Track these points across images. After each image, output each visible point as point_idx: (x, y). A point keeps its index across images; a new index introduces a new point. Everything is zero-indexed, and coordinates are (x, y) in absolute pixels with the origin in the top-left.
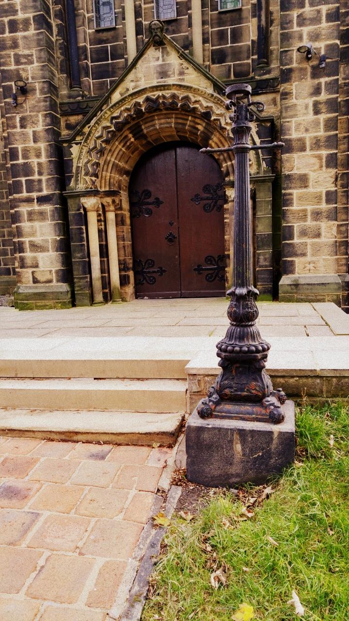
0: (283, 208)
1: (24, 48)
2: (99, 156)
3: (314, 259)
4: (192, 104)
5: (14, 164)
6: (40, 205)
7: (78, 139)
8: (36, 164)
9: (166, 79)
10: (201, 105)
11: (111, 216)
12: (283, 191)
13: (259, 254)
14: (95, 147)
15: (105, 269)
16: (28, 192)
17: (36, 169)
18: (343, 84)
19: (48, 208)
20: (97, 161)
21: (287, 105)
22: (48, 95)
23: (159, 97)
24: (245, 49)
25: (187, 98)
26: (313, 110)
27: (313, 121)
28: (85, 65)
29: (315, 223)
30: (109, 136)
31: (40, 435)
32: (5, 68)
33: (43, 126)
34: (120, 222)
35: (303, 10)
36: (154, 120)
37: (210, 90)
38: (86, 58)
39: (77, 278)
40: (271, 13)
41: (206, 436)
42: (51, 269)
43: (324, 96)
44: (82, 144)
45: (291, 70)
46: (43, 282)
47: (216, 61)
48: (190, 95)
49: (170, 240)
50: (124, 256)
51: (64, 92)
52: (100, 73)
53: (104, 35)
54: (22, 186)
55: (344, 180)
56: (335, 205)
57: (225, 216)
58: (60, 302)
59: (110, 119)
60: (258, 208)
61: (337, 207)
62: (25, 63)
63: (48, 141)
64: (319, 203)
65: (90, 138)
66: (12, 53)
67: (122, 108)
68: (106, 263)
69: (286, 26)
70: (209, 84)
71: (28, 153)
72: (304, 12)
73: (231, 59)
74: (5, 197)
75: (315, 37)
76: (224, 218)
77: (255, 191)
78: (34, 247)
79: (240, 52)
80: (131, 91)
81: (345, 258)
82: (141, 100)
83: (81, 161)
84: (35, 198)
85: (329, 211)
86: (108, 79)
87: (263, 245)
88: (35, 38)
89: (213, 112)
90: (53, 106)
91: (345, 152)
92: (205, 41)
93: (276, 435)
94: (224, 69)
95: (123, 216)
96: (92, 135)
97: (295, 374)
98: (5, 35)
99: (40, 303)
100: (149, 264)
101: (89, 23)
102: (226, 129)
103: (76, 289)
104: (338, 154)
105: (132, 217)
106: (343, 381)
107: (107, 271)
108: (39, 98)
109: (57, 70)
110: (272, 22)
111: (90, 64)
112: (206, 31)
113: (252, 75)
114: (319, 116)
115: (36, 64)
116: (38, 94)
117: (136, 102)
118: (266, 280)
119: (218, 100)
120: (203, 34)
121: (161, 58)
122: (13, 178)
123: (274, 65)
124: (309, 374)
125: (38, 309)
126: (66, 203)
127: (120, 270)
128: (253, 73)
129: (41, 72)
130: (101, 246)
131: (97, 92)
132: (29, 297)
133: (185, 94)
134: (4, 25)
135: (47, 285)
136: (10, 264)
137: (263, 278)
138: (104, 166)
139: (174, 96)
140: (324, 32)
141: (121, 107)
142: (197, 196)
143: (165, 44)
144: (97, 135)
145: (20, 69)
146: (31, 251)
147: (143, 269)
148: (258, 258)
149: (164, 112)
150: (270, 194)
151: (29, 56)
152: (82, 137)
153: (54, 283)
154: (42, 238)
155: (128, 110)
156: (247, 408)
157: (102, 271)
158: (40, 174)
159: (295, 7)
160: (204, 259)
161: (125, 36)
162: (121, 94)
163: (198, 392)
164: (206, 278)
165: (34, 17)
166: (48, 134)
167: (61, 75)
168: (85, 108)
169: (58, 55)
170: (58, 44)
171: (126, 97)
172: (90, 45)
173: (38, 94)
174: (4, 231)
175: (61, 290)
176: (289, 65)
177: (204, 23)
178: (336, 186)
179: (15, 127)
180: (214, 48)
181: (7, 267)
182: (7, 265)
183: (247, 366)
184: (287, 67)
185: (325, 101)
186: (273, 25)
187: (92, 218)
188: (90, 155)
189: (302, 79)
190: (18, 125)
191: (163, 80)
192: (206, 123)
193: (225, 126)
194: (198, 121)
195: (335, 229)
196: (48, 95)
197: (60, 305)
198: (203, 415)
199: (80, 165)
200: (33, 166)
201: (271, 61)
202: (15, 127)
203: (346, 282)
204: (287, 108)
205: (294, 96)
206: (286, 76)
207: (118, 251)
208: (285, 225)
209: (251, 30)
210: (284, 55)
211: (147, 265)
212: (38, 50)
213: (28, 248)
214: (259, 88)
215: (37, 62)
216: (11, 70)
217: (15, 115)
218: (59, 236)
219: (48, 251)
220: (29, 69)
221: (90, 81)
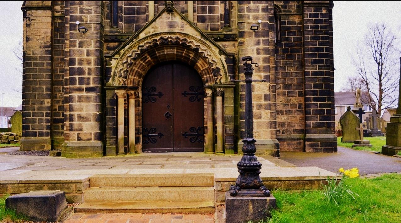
0: (240, 102)
2: (129, 67)
4: (188, 43)
5: (72, 68)
7: (116, 56)
8: (87, 68)
9: (173, 29)
10: (193, 44)
11: (132, 101)
12: (240, 93)
13: (226, 127)
14: (127, 62)
16: (79, 84)
18: (271, 41)
19: (93, 95)
20: (128, 69)
21: (242, 49)
22: (99, 31)
23: (168, 38)
24: (217, 17)
26: (257, 52)
27: (256, 58)
28: (121, 16)
29: (258, 111)
30: (136, 56)
31: (141, 211)
32: (73, 15)
34: (137, 104)
35: (249, 5)
36: (164, 49)
37: (199, 37)
38: (122, 13)
41: (236, 203)
42: (91, 132)
43: (261, 46)
44: (119, 59)
45: (244, 32)
46: (85, 140)
47: (200, 21)
48: (187, 39)
50: (138, 125)
55: (273, 89)
56: (269, 102)
57: (204, 104)
58: (96, 153)
59: (137, 46)
60: (225, 101)
61: (270, 103)
63: (96, 56)
64: (260, 100)
65: (124, 56)
66: (79, 7)
69: (241, 11)
71: (82, 62)
72: (250, 6)
73: (209, 21)
75: (257, 18)
76: (203, 106)
77: (224, 92)
78: (81, 118)
79: (214, 19)
80: (151, 33)
83: (117, 69)
84: (85, 88)
85: (266, 105)
86: (134, 24)
87: (229, 122)
90: (101, 37)
92: (194, 11)
94: (204, 25)
95: (139, 101)
96: (125, 55)
99: (82, 153)
100: (153, 131)
103: (107, 145)
104: (270, 75)
106: (291, 182)
108: (93, 32)
109: (104, 17)
111: (123, 15)
112: (195, 6)
113: (220, 31)
114: (259, 56)
115: (93, 14)
116: (93, 30)
117: (155, 39)
118: (230, 142)
119: (203, 42)
120: (194, 8)
121: (170, 18)
122: (70, 75)
123: (234, 27)
125: (80, 157)
126: (105, 93)
127: (136, 134)
129: (96, 19)
130: (125, 119)
131: (126, 30)
133: (184, 38)
136: (37, 129)
137: (229, 141)
138: (130, 72)
139: (177, 38)
141: (144, 41)
143: (173, 12)
144: (129, 55)
146: (78, 120)
152: (119, 56)
154: (87, 113)
155: (150, 43)
156: (253, 192)
158: (89, 74)
160: (189, 128)
162: (146, 34)
163: (221, 190)
164: (190, 140)
166: (97, 52)
167: (107, 20)
170: (106, 4)
171: (148, 36)
172: (124, 6)
174: (35, 107)
175: (97, 145)
176: (243, 29)
178: (270, 91)
179: (75, 46)
180: (199, 15)
181: (35, 131)
182: (34, 130)
184: (242, 30)
185: (262, 48)
186: (233, 9)
187: (121, 101)
188: (123, 66)
190: (77, 45)
191: (171, 29)
192: (195, 53)
195: (269, 114)
196: (99, 31)
197: (96, 155)
198: (232, 195)
199: (116, 71)
200: (85, 69)
202: (75, 46)
203: (276, 144)
204: (242, 50)
206: (242, 34)
207: (135, 122)
208: (241, 111)
212: (96, 7)
213: (76, 119)
214: (226, 38)
215: (94, 13)
217: (76, 40)
218: (98, 112)
219: (90, 121)
221: (122, 24)
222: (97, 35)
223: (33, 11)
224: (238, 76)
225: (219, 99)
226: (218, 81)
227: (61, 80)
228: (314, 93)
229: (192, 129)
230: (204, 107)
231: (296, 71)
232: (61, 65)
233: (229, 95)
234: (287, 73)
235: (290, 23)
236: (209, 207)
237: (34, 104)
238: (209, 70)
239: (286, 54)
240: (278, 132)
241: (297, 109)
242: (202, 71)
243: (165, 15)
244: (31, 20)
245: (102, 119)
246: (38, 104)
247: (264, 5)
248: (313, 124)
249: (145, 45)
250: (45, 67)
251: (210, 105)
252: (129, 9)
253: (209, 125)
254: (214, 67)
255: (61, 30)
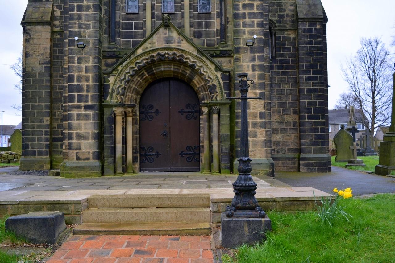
0: (236, 120)
1: (85, 20)
2: (126, 83)
3: (253, 149)
5: (70, 85)
6: (86, 110)
7: (114, 72)
10: (190, 60)
12: (236, 111)
13: (222, 146)
14: (124, 79)
15: (124, 152)
17: (85, 89)
19: (91, 113)
23: (165, 54)
25: (182, 56)
27: (252, 75)
28: (119, 31)
29: (253, 129)
33: (92, 64)
35: (245, 20)
37: (195, 53)
38: (120, 28)
39: (107, 157)
40: (228, 18)
42: (89, 151)
43: (257, 62)
45: (239, 48)
46: (83, 160)
47: (196, 37)
48: (184, 55)
49: (164, 135)
51: (105, 45)
52: (127, 36)
53: (131, 16)
54: (75, 98)
56: (264, 120)
57: (201, 123)
58: (95, 173)
59: (135, 63)
60: (221, 119)
62: (85, 28)
63: (95, 73)
65: (122, 73)
66: (77, 22)
67: (143, 58)
68: (125, 147)
69: (236, 26)
70: (194, 50)
74: (38, 101)
75: (252, 33)
76: (200, 124)
77: (220, 110)
78: (79, 136)
79: (210, 34)
80: (149, 49)
81: (270, 150)
82: (155, 54)
83: (115, 86)
85: (261, 123)
88: (93, 16)
89: (197, 65)
91: (268, 91)
92: (191, 26)
93: (263, 222)
96: (123, 71)
97: (264, 200)
98: (74, 12)
99: (80, 173)
100: (150, 150)
101: (122, 9)
102: (204, 74)
103: (105, 164)
105: (140, 120)
106: (286, 203)
107: (125, 154)
108: (91, 48)
110: (228, 22)
111: (121, 31)
113: (216, 46)
115: (91, 29)
116: (91, 46)
120: (190, 23)
121: (167, 34)
123: (230, 43)
124: (271, 200)
127: (133, 153)
128: (218, 45)
129: (94, 34)
130: (123, 137)
132: (72, 169)
133: (181, 54)
134: (74, 7)
135: (86, 161)
136: (36, 148)
139: (174, 54)
140: (256, 32)
142: (182, 109)
145: (81, 31)
146: (77, 139)
147: (146, 153)
148: (222, 148)
149: (167, 62)
150: (228, 112)
151: (88, 24)
152: (116, 72)
153: (91, 160)
156: (249, 212)
157: (123, 153)
158: (88, 91)
159: (241, 18)
161: (145, 19)
165: (93, 5)
168: (119, 55)
169: (104, 25)
171: (146, 52)
173: (91, 46)
174: (34, 125)
175: (96, 165)
176: (238, 45)
177: (191, 17)
179: (73, 63)
180: (195, 30)
181: (34, 150)
183: (248, 193)
187: (119, 119)
189: (245, 53)
190: (76, 62)
193: (203, 73)
194: (187, 68)
195: (264, 133)
199: (114, 88)
201: (228, 41)
202: (73, 63)
204: (238, 66)
205: (241, 61)
206: (237, 50)
207: (133, 141)
209: (216, 25)
210: (236, 40)
211: (148, 150)
214: (222, 54)
215: (92, 28)
216: (75, 31)
217: (74, 56)
218: (97, 130)
220: (87, 31)
221: (120, 40)
222: (95, 51)
223: (32, 26)
224: (234, 93)
225: (215, 117)
226: (214, 98)
227: (60, 97)
228: (309, 111)
229: (189, 148)
230: (201, 125)
231: (291, 88)
232: (60, 82)
233: (225, 113)
234: (281, 90)
235: (284, 38)
236: (205, 228)
237: (34, 122)
238: (205, 87)
239: (281, 71)
240: (273, 151)
241: (292, 127)
242: (199, 88)
243: (162, 30)
244: (31, 35)
245: (100, 137)
246: (37, 122)
247: (259, 20)
248: (307, 143)
249: (143, 61)
250: (44, 84)
251: (207, 124)
252: (126, 24)
253: (205, 143)
254: (210, 84)
255: (59, 46)
